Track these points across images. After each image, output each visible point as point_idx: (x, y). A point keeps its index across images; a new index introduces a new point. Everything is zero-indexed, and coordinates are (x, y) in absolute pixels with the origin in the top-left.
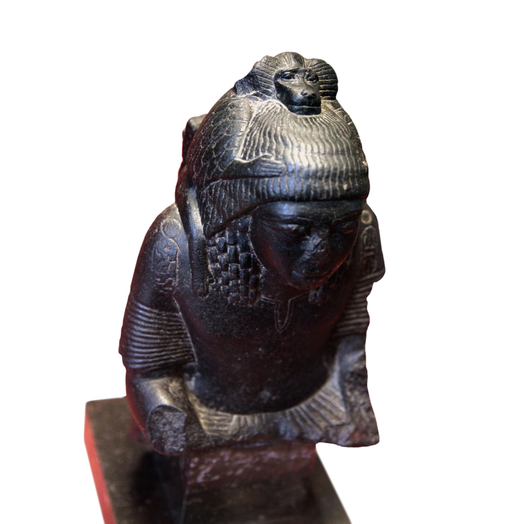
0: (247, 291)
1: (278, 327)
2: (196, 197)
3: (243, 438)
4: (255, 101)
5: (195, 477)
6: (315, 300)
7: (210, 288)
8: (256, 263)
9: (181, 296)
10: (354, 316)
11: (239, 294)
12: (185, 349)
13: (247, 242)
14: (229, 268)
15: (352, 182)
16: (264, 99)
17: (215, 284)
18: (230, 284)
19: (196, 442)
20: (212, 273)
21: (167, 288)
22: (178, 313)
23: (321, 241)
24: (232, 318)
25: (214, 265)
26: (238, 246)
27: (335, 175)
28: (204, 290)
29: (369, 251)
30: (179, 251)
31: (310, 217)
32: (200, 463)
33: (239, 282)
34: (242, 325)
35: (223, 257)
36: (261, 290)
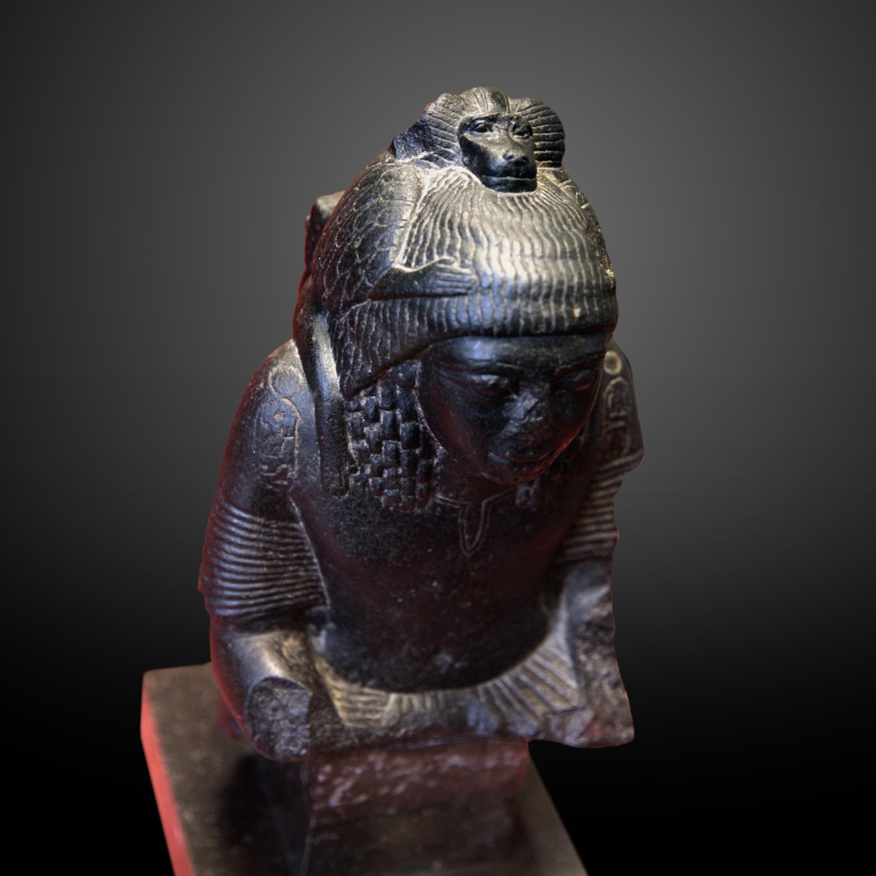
0: (413, 486)
1: (465, 547)
2: (327, 329)
3: (406, 733)
4: (427, 169)
5: (326, 797)
6: (526, 501)
7: (352, 482)
8: (427, 440)
10: (592, 528)
11: (399, 491)
12: (309, 584)
13: (412, 404)
14: (383, 448)
15: (589, 303)
16: (442, 165)
17: (360, 475)
18: (385, 475)
19: (328, 738)
20: (354, 456)
21: (279, 482)
22: (298, 523)
23: (537, 403)
24: (388, 532)
25: (358, 443)
26: (398, 412)
27: (559, 292)
28: (341, 485)
29: (617, 419)
30: (300, 419)
31: (519, 362)
32: (335, 774)
33: (400, 471)
34: (404, 543)
35: (372, 430)
36: (437, 485)
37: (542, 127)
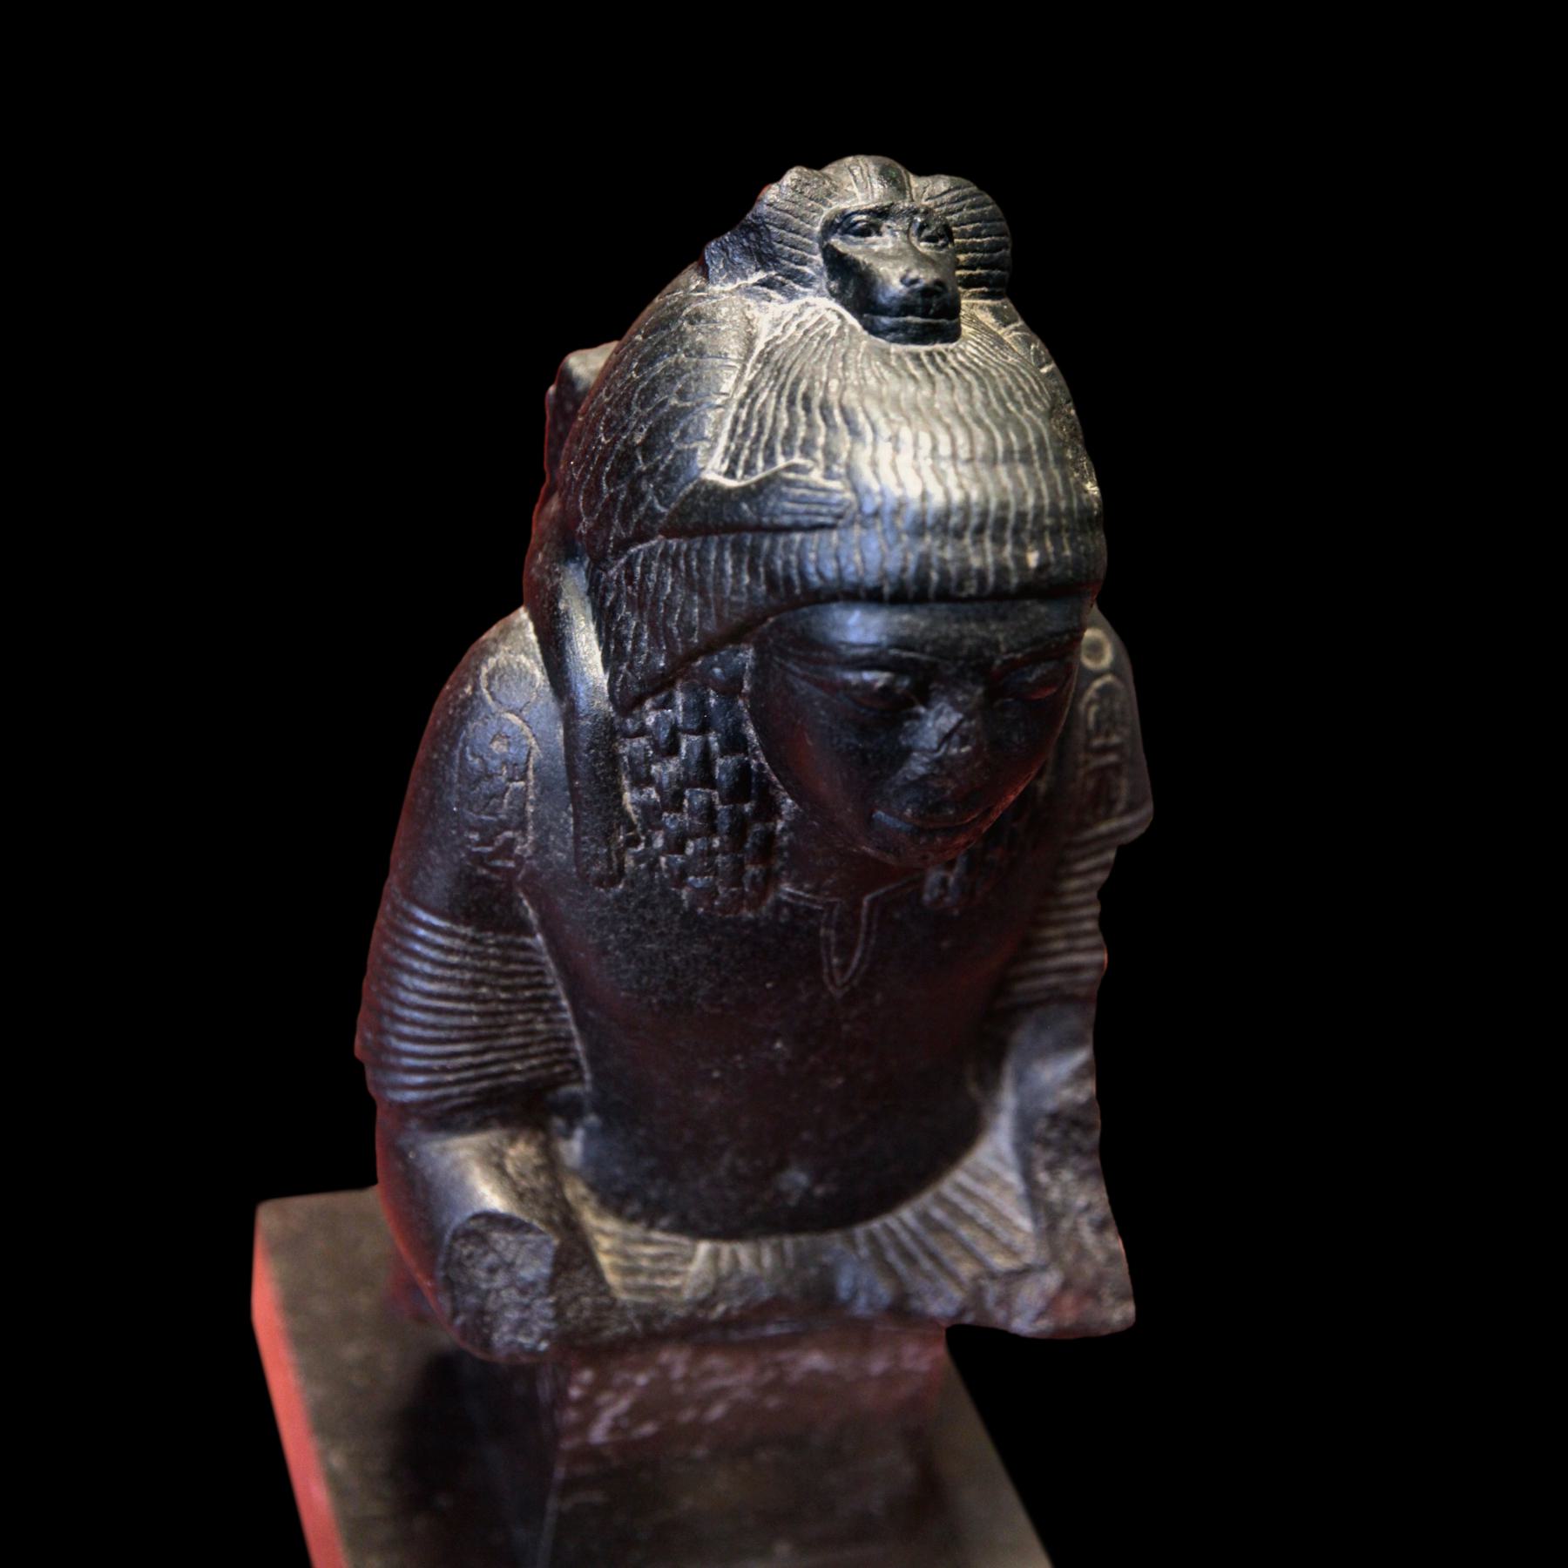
0: (739, 869)
1: (832, 979)
2: (585, 589)
3: (727, 1312)
4: (764, 303)
5: (584, 1426)
6: (941, 897)
7: (630, 862)
8: (765, 787)
9: (540, 885)
11: (715, 880)
12: (553, 1045)
13: (738, 723)
14: (686, 803)
15: (1054, 543)
16: (791, 295)
17: (644, 850)
18: (689, 851)
19: (587, 1321)
20: (634, 817)
21: (499, 863)
22: (533, 935)
23: (960, 722)
24: (694, 952)
25: (641, 793)
26: (712, 738)
27: (1001, 523)
28: (610, 868)
29: (1105, 750)
30: (536, 750)
31: (929, 648)
32: (600, 1385)
33: (716, 843)
34: (723, 973)
35: (666, 770)
36: (782, 868)
37: (970, 227)
